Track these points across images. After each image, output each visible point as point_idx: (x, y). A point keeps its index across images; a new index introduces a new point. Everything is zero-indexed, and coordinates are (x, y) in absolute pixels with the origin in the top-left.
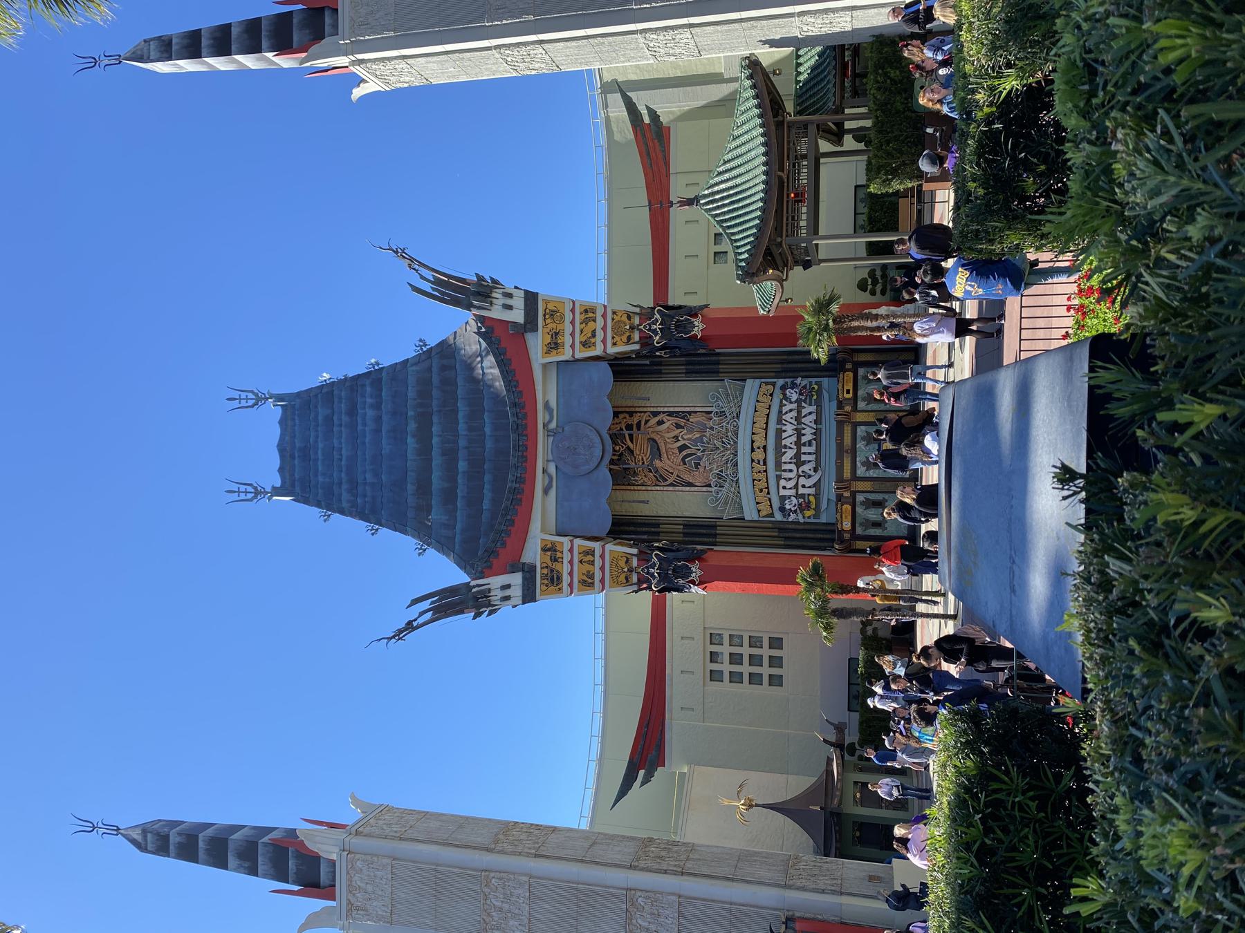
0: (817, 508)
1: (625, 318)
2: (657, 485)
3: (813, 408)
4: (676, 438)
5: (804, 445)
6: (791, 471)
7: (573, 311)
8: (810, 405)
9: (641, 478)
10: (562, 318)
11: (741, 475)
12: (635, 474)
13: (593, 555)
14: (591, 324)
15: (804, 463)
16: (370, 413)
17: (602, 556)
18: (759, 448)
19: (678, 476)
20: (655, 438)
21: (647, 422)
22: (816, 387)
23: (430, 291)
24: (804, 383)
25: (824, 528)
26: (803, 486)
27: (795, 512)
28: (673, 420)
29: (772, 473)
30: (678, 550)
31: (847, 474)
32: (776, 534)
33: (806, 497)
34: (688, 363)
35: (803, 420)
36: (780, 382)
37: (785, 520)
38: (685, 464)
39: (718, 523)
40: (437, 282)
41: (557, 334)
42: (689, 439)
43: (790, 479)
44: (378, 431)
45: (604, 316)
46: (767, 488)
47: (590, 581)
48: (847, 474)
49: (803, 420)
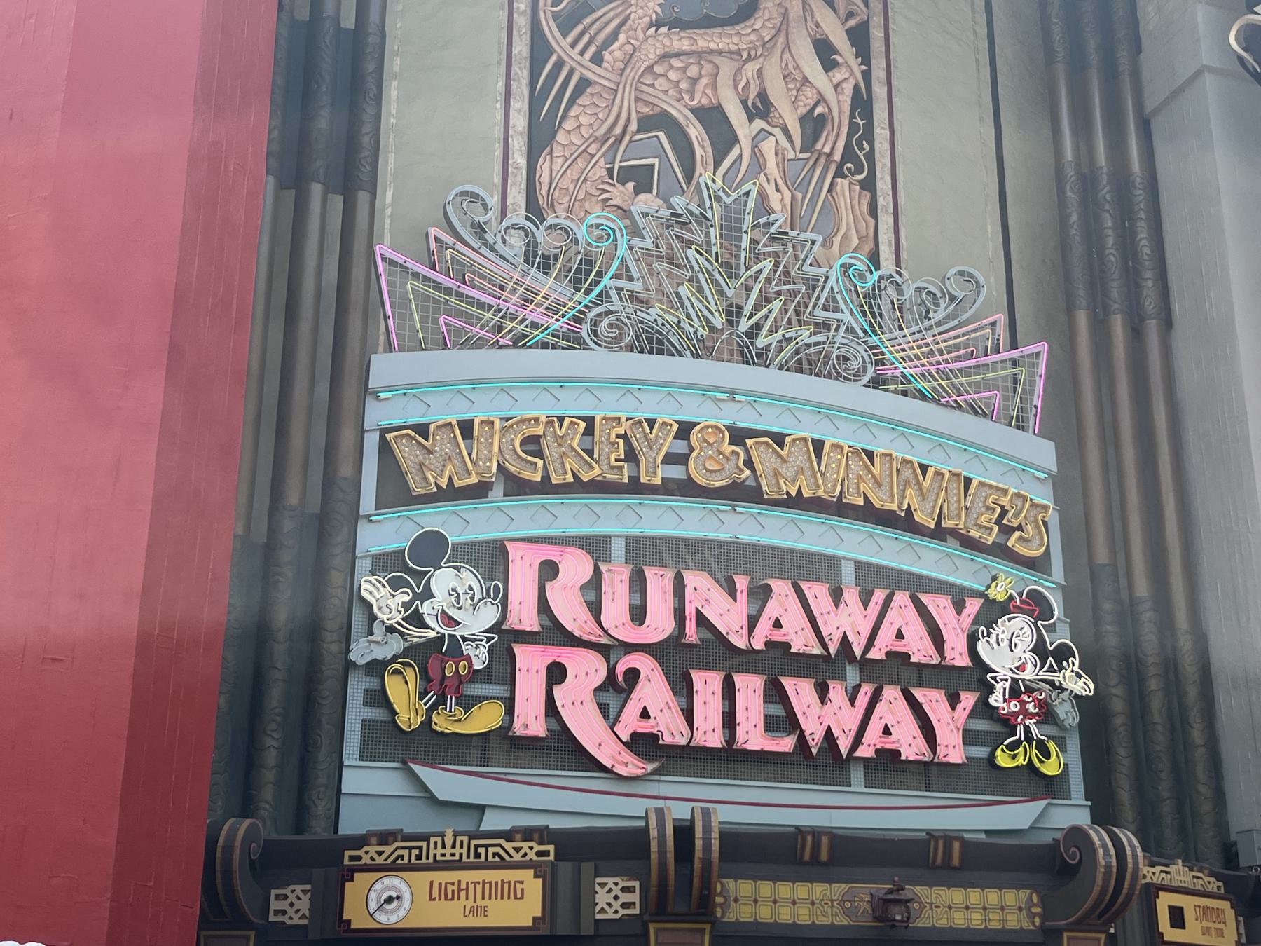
4: (760, 108)
5: (775, 692)
6: (638, 614)
8: (969, 737)
15: (683, 687)
19: (584, 84)
26: (556, 674)
28: (841, 105)
35: (891, 693)
37: (363, 565)
38: (646, 124)
43: (595, 609)
46: (545, 487)
49: (891, 693)
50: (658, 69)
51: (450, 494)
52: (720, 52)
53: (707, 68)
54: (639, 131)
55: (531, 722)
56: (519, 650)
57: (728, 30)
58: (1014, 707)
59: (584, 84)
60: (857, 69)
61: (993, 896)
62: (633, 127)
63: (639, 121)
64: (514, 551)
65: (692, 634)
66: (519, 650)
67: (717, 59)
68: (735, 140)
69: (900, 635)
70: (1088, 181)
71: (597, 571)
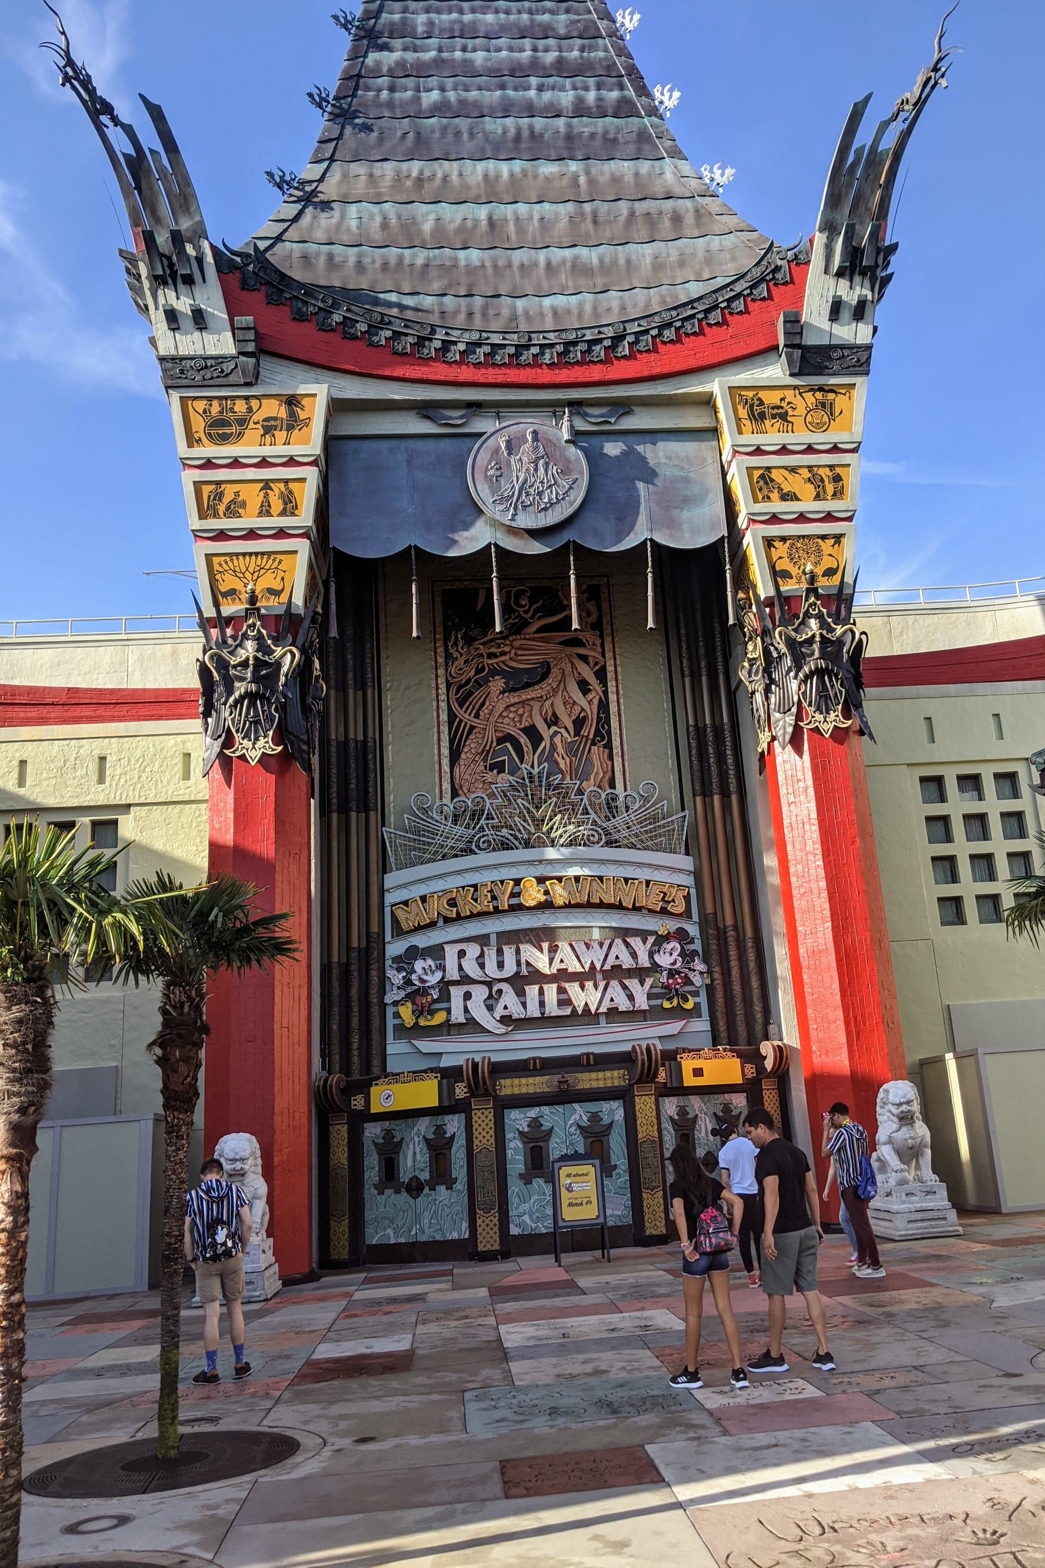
0: (418, 1031)
1: (828, 563)
2: (449, 686)
3: (642, 1002)
4: (553, 721)
5: (561, 991)
6: (501, 965)
7: (835, 449)
8: (650, 996)
9: (461, 653)
10: (820, 427)
11: (483, 858)
12: (469, 641)
13: (283, 513)
14: (810, 490)
15: (521, 993)
16: (567, 98)
17: (281, 534)
18: (546, 893)
19: (472, 728)
20: (552, 676)
21: (584, 658)
22: (689, 1005)
23: (856, 144)
24: (697, 980)
25: (375, 1050)
26: (468, 996)
27: (408, 982)
28: (592, 711)
29: (492, 926)
30: (306, 709)
31: (510, 1086)
32: (355, 943)
33: (444, 1005)
34: (718, 730)
35: (614, 983)
36: (693, 930)
37: (388, 963)
38: (500, 741)
39: (372, 814)
40: (874, 158)
41: (784, 417)
42: (553, 748)
43: (482, 966)
44: (531, 111)
45: (829, 517)
46: (459, 918)
47: (221, 508)
48: (510, 1086)
49: (614, 983)
50: (504, 714)
51: (419, 928)
52: (533, 699)
53: (527, 708)
54: (498, 745)
55: (458, 1016)
56: (451, 988)
57: (536, 687)
58: (671, 981)
59: (472, 728)
60: (599, 689)
61: (608, 1074)
62: (494, 744)
63: (497, 740)
64: (447, 948)
65: (524, 971)
66: (451, 988)
67: (532, 703)
68: (542, 739)
69: (617, 957)
70: (700, 732)
71: (482, 950)
